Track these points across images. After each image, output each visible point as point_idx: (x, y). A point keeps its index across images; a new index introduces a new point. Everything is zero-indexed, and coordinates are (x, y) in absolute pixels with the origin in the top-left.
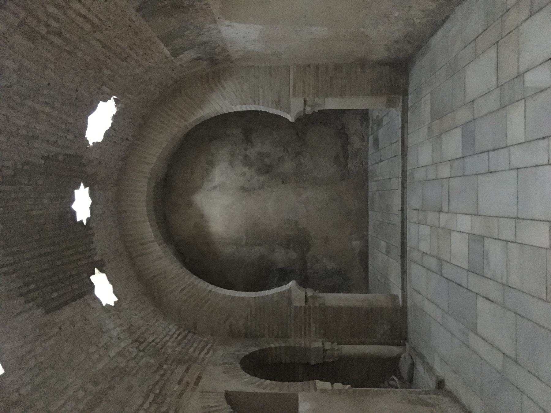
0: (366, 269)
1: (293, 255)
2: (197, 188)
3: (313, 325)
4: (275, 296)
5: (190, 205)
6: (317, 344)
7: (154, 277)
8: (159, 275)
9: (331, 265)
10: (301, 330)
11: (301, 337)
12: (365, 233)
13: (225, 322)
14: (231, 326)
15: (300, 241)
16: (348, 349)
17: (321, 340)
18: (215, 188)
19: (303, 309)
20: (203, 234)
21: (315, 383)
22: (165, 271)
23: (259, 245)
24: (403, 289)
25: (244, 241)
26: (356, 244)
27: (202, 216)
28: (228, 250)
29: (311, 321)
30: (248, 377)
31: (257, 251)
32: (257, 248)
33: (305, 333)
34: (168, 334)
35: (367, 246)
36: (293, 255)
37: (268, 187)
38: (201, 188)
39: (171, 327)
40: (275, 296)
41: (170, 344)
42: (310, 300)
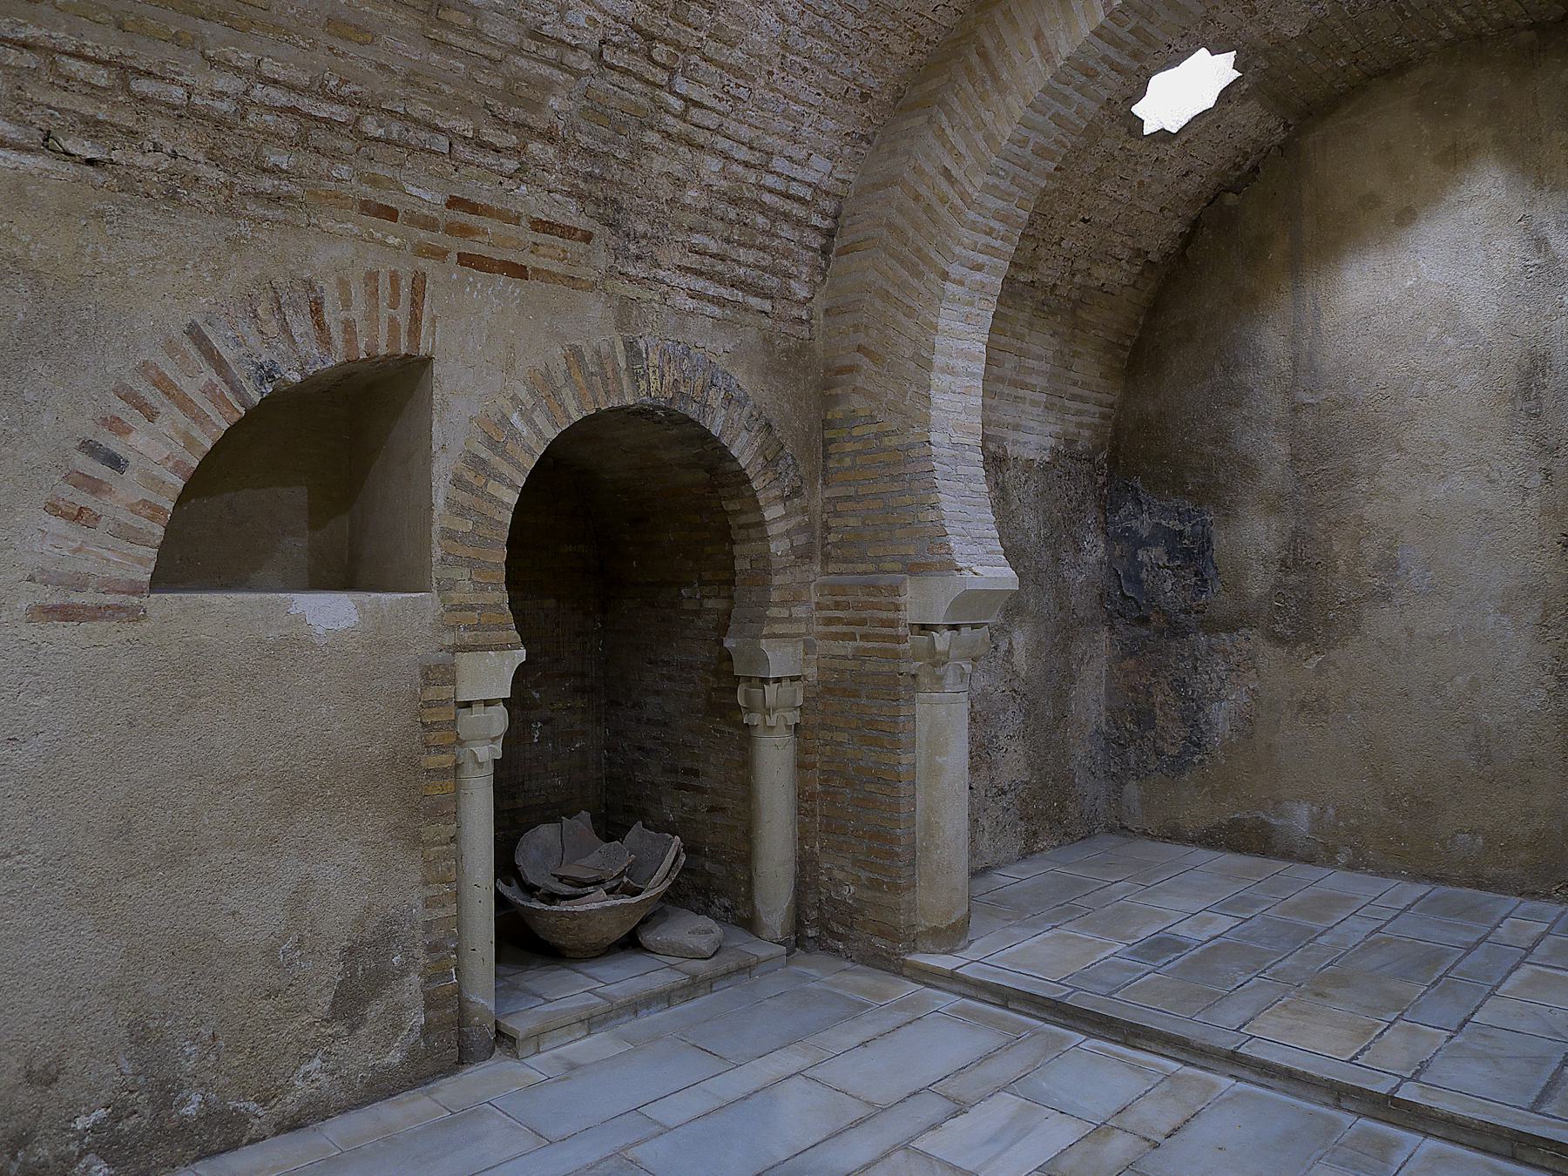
0: (1210, 839)
1: (1258, 584)
2: (1530, 162)
3: (849, 647)
4: (932, 515)
5: (1455, 158)
6: (780, 658)
7: (984, 55)
8: (995, 78)
9: (1221, 717)
10: (837, 606)
11: (819, 607)
12: (1342, 859)
13: (860, 349)
14: (851, 369)
15: (1309, 611)
16: (775, 762)
17: (812, 672)
18: (1541, 243)
19: (891, 615)
20: (1323, 236)
21: (501, 648)
22: (1003, 90)
23: (1295, 458)
24: (952, 979)
25: (1307, 398)
26: (1299, 819)
27: (1406, 217)
28: (1272, 339)
29: (860, 643)
30: (534, 435)
31: (1273, 453)
32: (1282, 449)
33: (829, 621)
34: (770, 154)
35: (1287, 855)
36: (1258, 584)
37: (1548, 474)
38: (1539, 184)
39: (820, 163)
40: (932, 515)
41: (714, 164)
42: (923, 640)
